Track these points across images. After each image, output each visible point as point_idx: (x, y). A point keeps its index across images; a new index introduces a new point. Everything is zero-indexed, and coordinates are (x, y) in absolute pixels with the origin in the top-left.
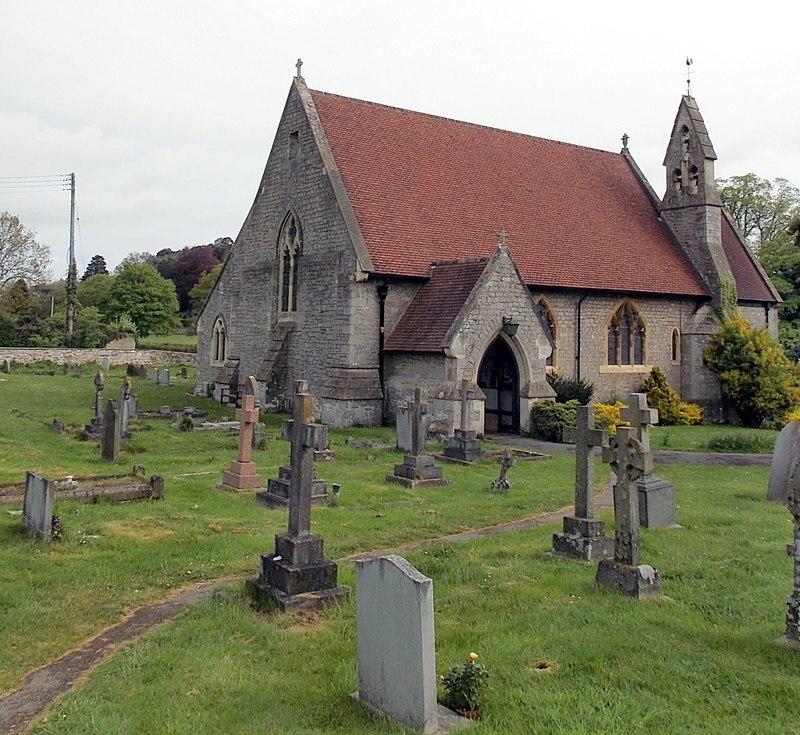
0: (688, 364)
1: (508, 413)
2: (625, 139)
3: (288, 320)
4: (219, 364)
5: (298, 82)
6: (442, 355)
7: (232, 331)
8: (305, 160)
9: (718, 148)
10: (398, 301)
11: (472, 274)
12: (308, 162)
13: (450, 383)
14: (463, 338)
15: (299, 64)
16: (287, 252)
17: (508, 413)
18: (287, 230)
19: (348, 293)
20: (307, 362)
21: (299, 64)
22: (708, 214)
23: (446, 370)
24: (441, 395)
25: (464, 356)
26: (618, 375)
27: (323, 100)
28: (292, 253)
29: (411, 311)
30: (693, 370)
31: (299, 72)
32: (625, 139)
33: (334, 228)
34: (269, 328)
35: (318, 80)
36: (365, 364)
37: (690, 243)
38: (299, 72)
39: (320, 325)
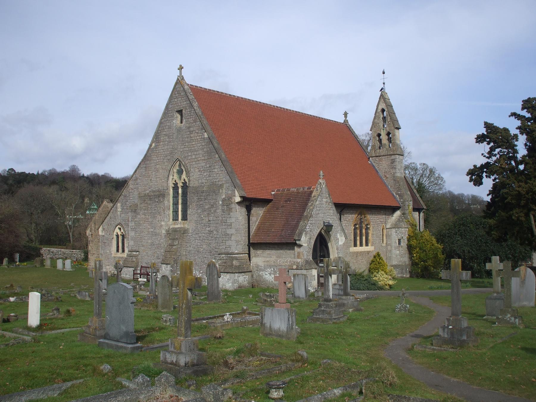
0: (390, 245)
1: (322, 277)
2: (346, 114)
3: (179, 226)
4: (120, 255)
5: (180, 82)
6: (295, 244)
7: (132, 234)
8: (189, 128)
9: (401, 123)
10: (258, 212)
11: (305, 199)
12: (192, 129)
13: (299, 260)
14: (306, 234)
15: (181, 68)
16: (176, 184)
17: (322, 277)
18: (175, 171)
19: (230, 210)
20: (198, 251)
21: (181, 68)
22: (398, 160)
23: (296, 252)
24: (295, 267)
25: (306, 245)
26: (357, 252)
27: (198, 91)
28: (180, 185)
29: (264, 219)
30: (393, 249)
31: (181, 73)
32: (346, 114)
33: (216, 170)
34: (164, 232)
35: (190, 79)
36: (241, 251)
37: (388, 176)
38: (181, 73)
39: (208, 229)
